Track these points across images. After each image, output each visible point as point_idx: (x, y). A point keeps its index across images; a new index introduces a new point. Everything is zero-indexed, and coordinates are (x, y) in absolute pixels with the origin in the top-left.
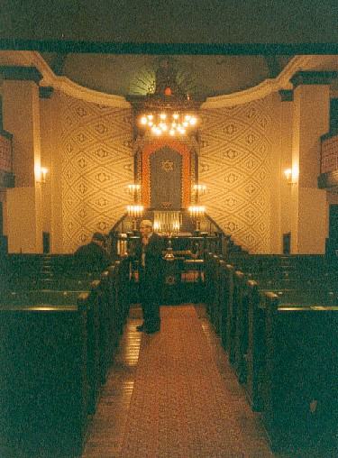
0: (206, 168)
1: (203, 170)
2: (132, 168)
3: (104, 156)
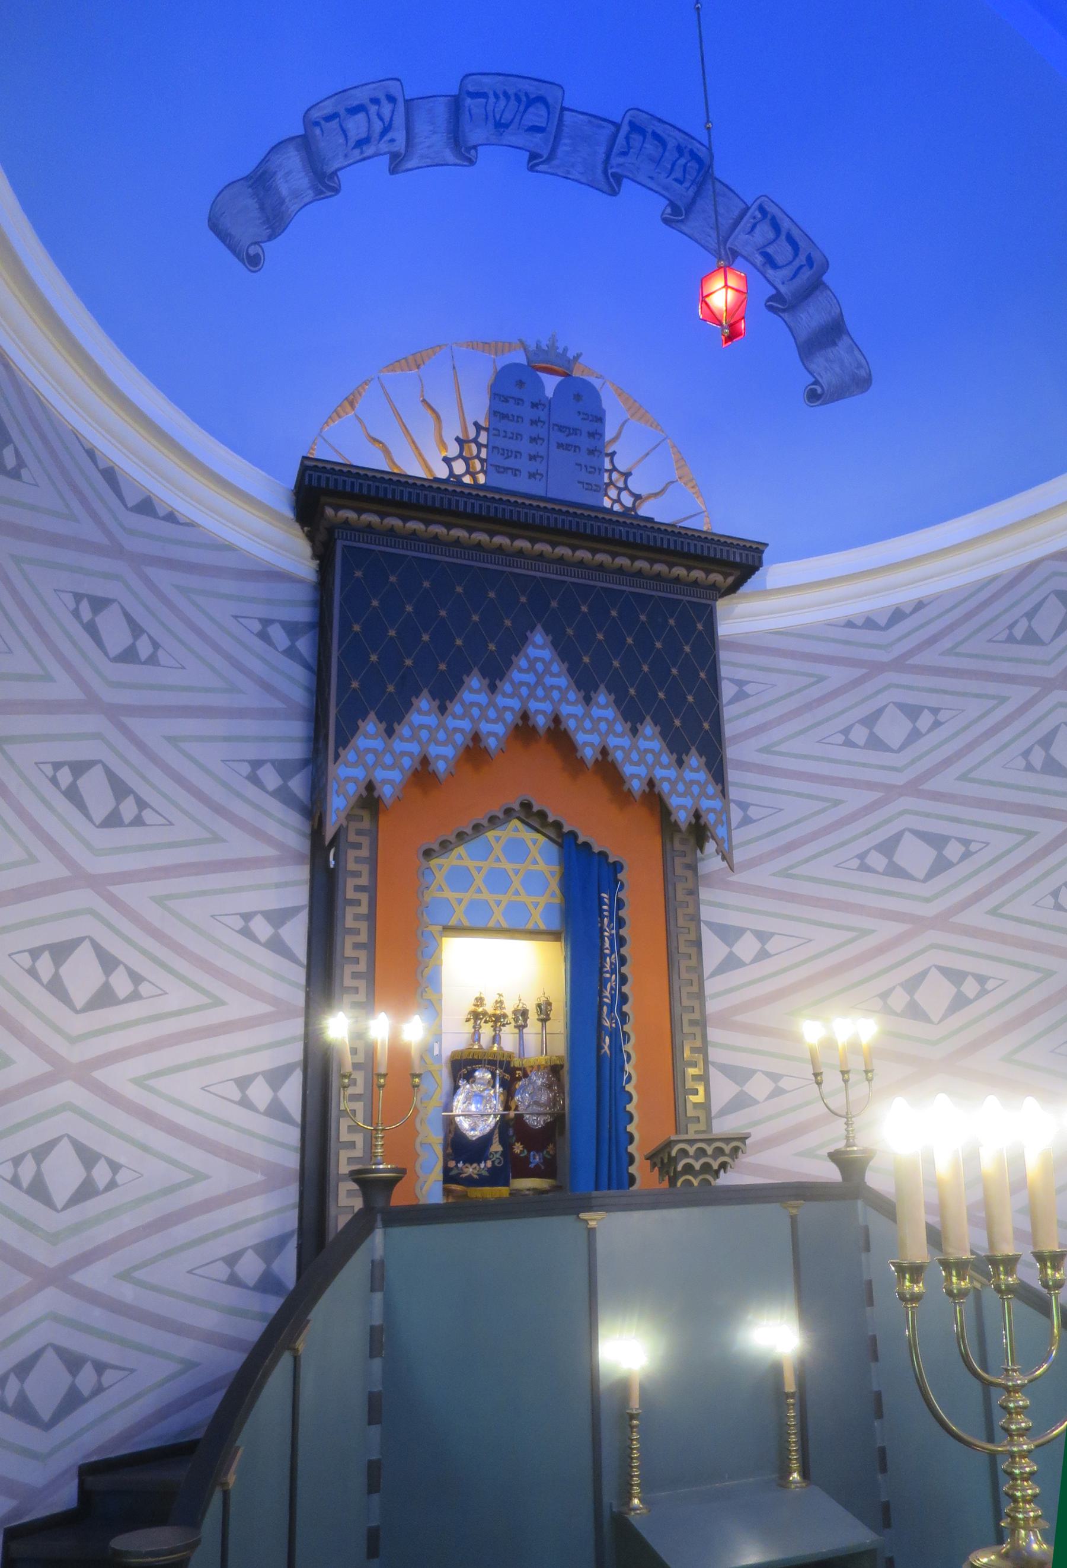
0: (745, 948)
1: (731, 963)
2: (296, 934)
3: (113, 820)
